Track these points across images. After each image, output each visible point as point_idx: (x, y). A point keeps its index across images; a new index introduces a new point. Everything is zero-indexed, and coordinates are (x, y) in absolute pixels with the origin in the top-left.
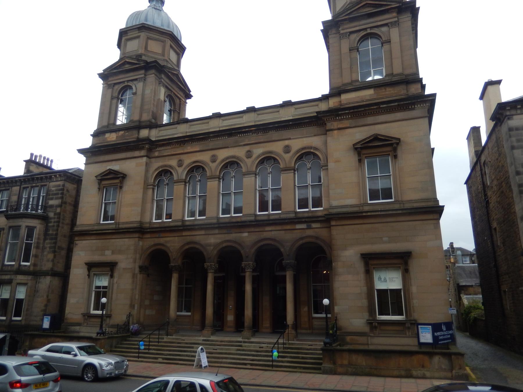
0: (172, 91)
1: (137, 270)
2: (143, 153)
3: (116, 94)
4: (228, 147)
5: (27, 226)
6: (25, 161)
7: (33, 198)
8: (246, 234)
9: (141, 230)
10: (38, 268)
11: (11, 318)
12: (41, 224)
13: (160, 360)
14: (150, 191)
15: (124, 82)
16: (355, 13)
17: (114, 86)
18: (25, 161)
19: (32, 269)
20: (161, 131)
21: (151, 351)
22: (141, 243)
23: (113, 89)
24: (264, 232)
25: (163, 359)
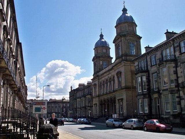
18: (145, 48)
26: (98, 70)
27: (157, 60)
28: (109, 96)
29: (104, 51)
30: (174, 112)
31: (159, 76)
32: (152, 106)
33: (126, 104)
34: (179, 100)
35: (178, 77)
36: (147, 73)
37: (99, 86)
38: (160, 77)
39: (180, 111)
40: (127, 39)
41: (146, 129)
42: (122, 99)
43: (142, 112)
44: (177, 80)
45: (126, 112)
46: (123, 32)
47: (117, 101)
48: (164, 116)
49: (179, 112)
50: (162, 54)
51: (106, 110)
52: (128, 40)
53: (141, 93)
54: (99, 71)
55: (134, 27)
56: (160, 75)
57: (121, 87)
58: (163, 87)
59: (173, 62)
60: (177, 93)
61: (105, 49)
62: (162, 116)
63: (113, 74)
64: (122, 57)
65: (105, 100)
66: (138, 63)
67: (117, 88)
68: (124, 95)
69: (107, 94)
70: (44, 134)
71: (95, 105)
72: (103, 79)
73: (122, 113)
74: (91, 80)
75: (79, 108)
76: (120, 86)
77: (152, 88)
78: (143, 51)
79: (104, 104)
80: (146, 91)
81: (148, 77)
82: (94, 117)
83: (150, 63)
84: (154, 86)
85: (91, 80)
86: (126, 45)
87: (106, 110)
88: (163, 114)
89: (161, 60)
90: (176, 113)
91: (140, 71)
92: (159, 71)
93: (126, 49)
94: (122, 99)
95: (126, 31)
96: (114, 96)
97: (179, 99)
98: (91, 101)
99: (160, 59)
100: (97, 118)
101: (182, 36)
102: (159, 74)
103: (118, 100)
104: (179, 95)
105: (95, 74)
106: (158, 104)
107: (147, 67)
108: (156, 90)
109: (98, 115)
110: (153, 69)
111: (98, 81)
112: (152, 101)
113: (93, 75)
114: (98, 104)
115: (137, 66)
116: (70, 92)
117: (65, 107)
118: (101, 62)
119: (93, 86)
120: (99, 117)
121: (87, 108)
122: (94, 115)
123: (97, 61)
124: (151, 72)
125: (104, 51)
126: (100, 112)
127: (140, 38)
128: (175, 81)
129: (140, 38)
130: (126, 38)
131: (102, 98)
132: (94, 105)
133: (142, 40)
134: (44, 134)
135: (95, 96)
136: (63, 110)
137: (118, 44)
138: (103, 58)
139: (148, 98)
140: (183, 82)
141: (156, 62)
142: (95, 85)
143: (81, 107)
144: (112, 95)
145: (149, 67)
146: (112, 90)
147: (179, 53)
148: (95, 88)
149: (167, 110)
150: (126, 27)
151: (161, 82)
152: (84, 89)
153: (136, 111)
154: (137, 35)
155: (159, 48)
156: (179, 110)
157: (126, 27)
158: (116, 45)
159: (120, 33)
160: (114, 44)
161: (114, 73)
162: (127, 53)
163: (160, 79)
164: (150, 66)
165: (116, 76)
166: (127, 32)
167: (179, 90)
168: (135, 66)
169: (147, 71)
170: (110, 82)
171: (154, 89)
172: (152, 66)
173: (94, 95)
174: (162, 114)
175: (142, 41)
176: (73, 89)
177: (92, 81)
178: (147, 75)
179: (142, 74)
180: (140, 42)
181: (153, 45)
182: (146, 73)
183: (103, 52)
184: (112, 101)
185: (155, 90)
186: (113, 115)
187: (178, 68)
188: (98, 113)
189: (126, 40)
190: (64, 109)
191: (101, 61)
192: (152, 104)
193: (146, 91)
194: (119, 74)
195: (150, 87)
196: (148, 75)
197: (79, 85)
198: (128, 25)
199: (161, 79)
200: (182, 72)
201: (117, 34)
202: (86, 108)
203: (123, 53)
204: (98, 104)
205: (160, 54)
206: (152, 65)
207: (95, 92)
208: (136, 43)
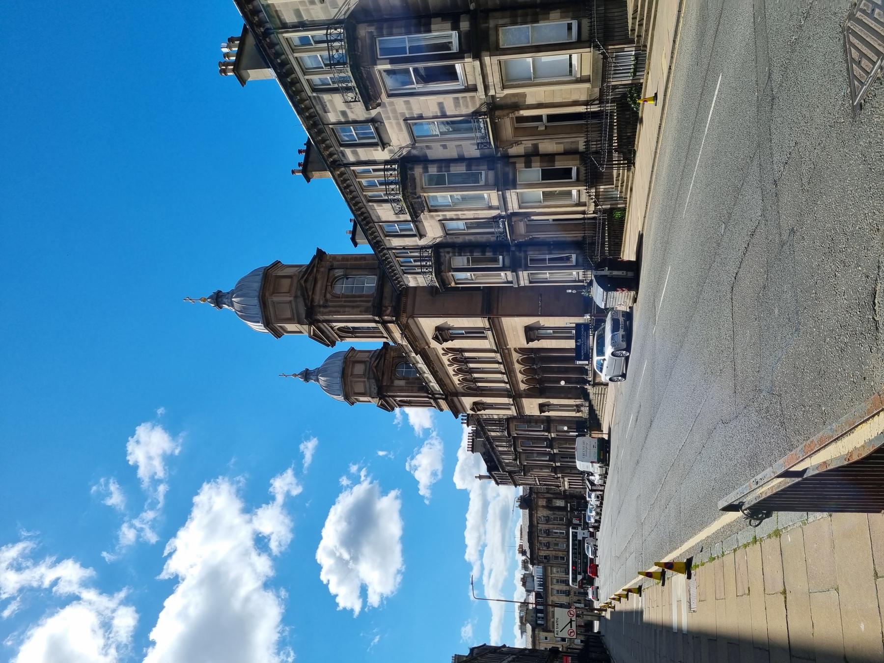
2: (455, 399)
29: (359, 369)
30: (578, 179)
34: (538, 158)
35: (461, 159)
36: (441, 250)
39: (578, 156)
40: (321, 303)
44: (470, 162)
46: (298, 313)
49: (578, 162)
51: (563, 383)
52: (326, 300)
55: (280, 273)
59: (409, 172)
60: (515, 163)
61: (353, 367)
63: (441, 352)
70: (381, 453)
71: (544, 409)
73: (574, 331)
74: (456, 417)
78: (365, 248)
79: (541, 381)
80: (501, 257)
85: (456, 417)
87: (563, 383)
90: (582, 169)
95: (293, 303)
97: (533, 158)
101: (250, 7)
103: (529, 340)
104: (523, 159)
107: (422, 248)
116: (498, 483)
117: (549, 500)
118: (397, 383)
125: (359, 369)
127: (320, 254)
128: (473, 168)
129: (320, 254)
130: (320, 306)
132: (544, 412)
133: (329, 251)
134: (381, 453)
136: (559, 508)
138: (385, 377)
139: (525, 252)
140: (478, 144)
142: (477, 406)
147: (379, 148)
154: (308, 266)
155: (360, 208)
156: (571, 163)
158: (340, 337)
162: (370, 304)
165: (449, 344)
166: (296, 297)
167: (506, 157)
170: (467, 360)
175: (330, 250)
176: (488, 474)
177: (460, 416)
178: (448, 253)
180: (334, 257)
183: (364, 375)
187: (430, 158)
189: (325, 307)
190: (560, 503)
191: (392, 382)
192: (548, 240)
193: (501, 257)
196: (449, 249)
197: (473, 451)
198: (273, 293)
200: (445, 147)
204: (541, 401)
206: (414, 232)
208: (336, 271)
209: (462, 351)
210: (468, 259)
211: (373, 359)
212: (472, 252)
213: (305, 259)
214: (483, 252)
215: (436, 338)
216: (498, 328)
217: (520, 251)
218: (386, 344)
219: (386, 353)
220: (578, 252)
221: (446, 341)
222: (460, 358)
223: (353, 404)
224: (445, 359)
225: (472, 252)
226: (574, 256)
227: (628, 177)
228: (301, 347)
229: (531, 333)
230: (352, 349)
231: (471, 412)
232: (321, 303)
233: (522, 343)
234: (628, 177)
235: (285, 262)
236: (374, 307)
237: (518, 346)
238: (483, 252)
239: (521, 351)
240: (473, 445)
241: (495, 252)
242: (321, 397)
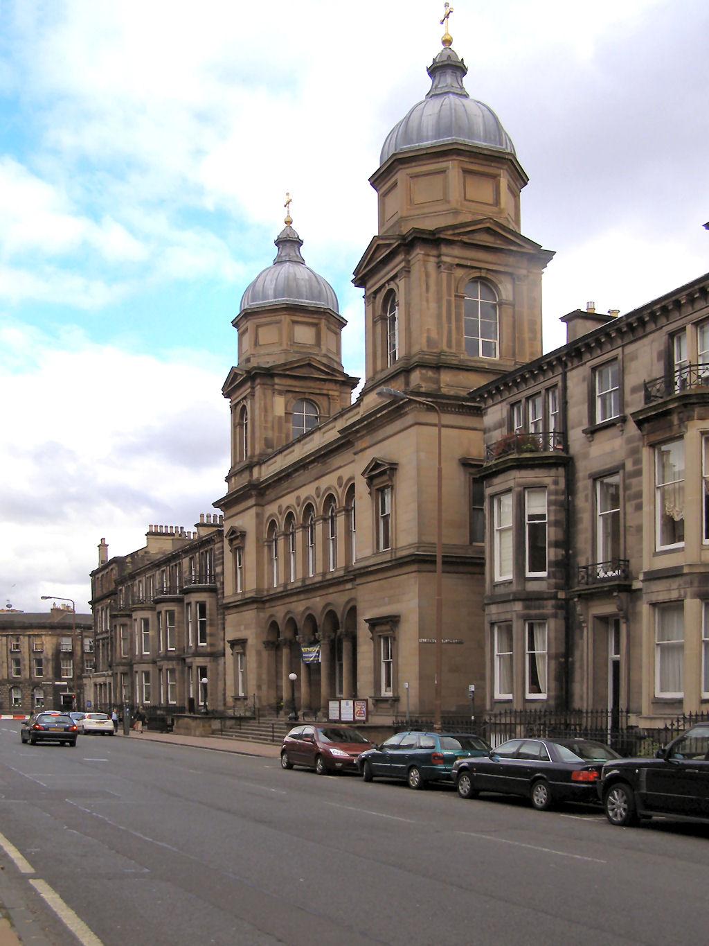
0: (480, 268)
1: (262, 647)
2: (252, 502)
3: (379, 312)
4: (305, 485)
5: (197, 602)
6: (563, 319)
7: (603, 398)
8: (318, 599)
9: (259, 601)
10: (214, 650)
11: (198, 703)
12: (210, 597)
13: (250, 739)
14: (266, 549)
15: (383, 286)
16: (377, 255)
17: (375, 298)
18: (563, 319)
19: (209, 650)
20: (306, 444)
21: (242, 731)
22: (262, 615)
23: (374, 303)
24: (329, 596)
25: (253, 738)
26: (257, 452)
27: (634, 390)
28: (317, 602)
31: (634, 490)
32: (577, 665)
33: (415, 645)
37: (258, 539)
38: (639, 495)
41: (540, 796)
42: (393, 621)
43: (510, 697)
45: (506, 419)
47: (363, 631)
48: (644, 725)
50: (668, 357)
53: (514, 588)
54: (261, 455)
56: (640, 484)
57: (395, 550)
58: (656, 554)
62: (633, 720)
63: (345, 473)
64: (406, 371)
65: (536, 711)
66: (505, 414)
67: (368, 552)
68: (408, 599)
69: (307, 589)
72: (288, 500)
73: (390, 694)
75: (142, 660)
76: (386, 546)
77: (582, 561)
81: (562, 498)
82: (230, 712)
83: (585, 408)
84: (596, 551)
86: (439, 300)
88: (639, 713)
89: (654, 391)
91: (518, 455)
92: (638, 462)
93: (439, 324)
94: (393, 621)
96: (348, 602)
98: (211, 625)
99: (646, 386)
100: (248, 714)
102: (634, 481)
103: (374, 623)
105: (241, 471)
106: (617, 652)
107: (563, 435)
108: (610, 573)
109: (250, 702)
110: (596, 454)
111: (258, 515)
112: (577, 633)
113: (228, 479)
114: (251, 641)
115: (499, 425)
117: (71, 655)
119: (226, 541)
120: (256, 715)
121: (188, 660)
122: (230, 700)
123: (252, 395)
124: (584, 469)
126: (264, 687)
131: (279, 612)
132: (232, 647)
135: (236, 593)
137: (384, 292)
141: (622, 405)
142: (237, 537)
143: (182, 649)
144: (338, 599)
145: (576, 436)
146: (341, 563)
148: (238, 550)
149: (662, 690)
150: (452, 197)
151: (639, 529)
152: (170, 560)
153: (472, 688)
157: (446, 198)
158: (376, 293)
159: (403, 219)
160: (362, 291)
161: (353, 467)
162: (445, 348)
163: (639, 507)
164: (584, 431)
165: (362, 487)
166: (456, 212)
168: (485, 431)
169: (565, 462)
171: (595, 564)
172: (593, 431)
173: (228, 590)
174: (633, 706)
176: (110, 558)
177: (219, 512)
178: (556, 483)
179: (529, 476)
180: (537, 284)
181: (623, 300)
182: (553, 472)
184: (338, 634)
185: (602, 575)
186: (333, 705)
188: (252, 690)
191: (280, 393)
192: (577, 654)
194: (382, 476)
195: (575, 555)
196: (562, 485)
199: (646, 508)
201: (381, 223)
202: (184, 660)
203: (415, 349)
205: (655, 355)
206: (599, 421)
207: (240, 576)
209: (349, 510)
210: (542, 517)
211: (324, 361)
212: (556, 523)
213: (530, 228)
214: (556, 544)
215: (376, 465)
216: (461, 569)
217: (557, 607)
218: (353, 382)
219: (336, 382)
220: (552, 702)
221: (370, 484)
222: (337, 506)
223: (236, 324)
224: (329, 481)
225: (556, 523)
226: (543, 696)
227: (267, 740)
228: (343, 228)
229: (386, 626)
230: (342, 323)
231: (226, 529)
232: (445, 259)
233: (367, 613)
234: (267, 740)
235: (525, 193)
236: (440, 354)
237: (361, 607)
238: (556, 544)
239: (353, 612)
240: (161, 534)
241: (556, 564)
242: (242, 269)
